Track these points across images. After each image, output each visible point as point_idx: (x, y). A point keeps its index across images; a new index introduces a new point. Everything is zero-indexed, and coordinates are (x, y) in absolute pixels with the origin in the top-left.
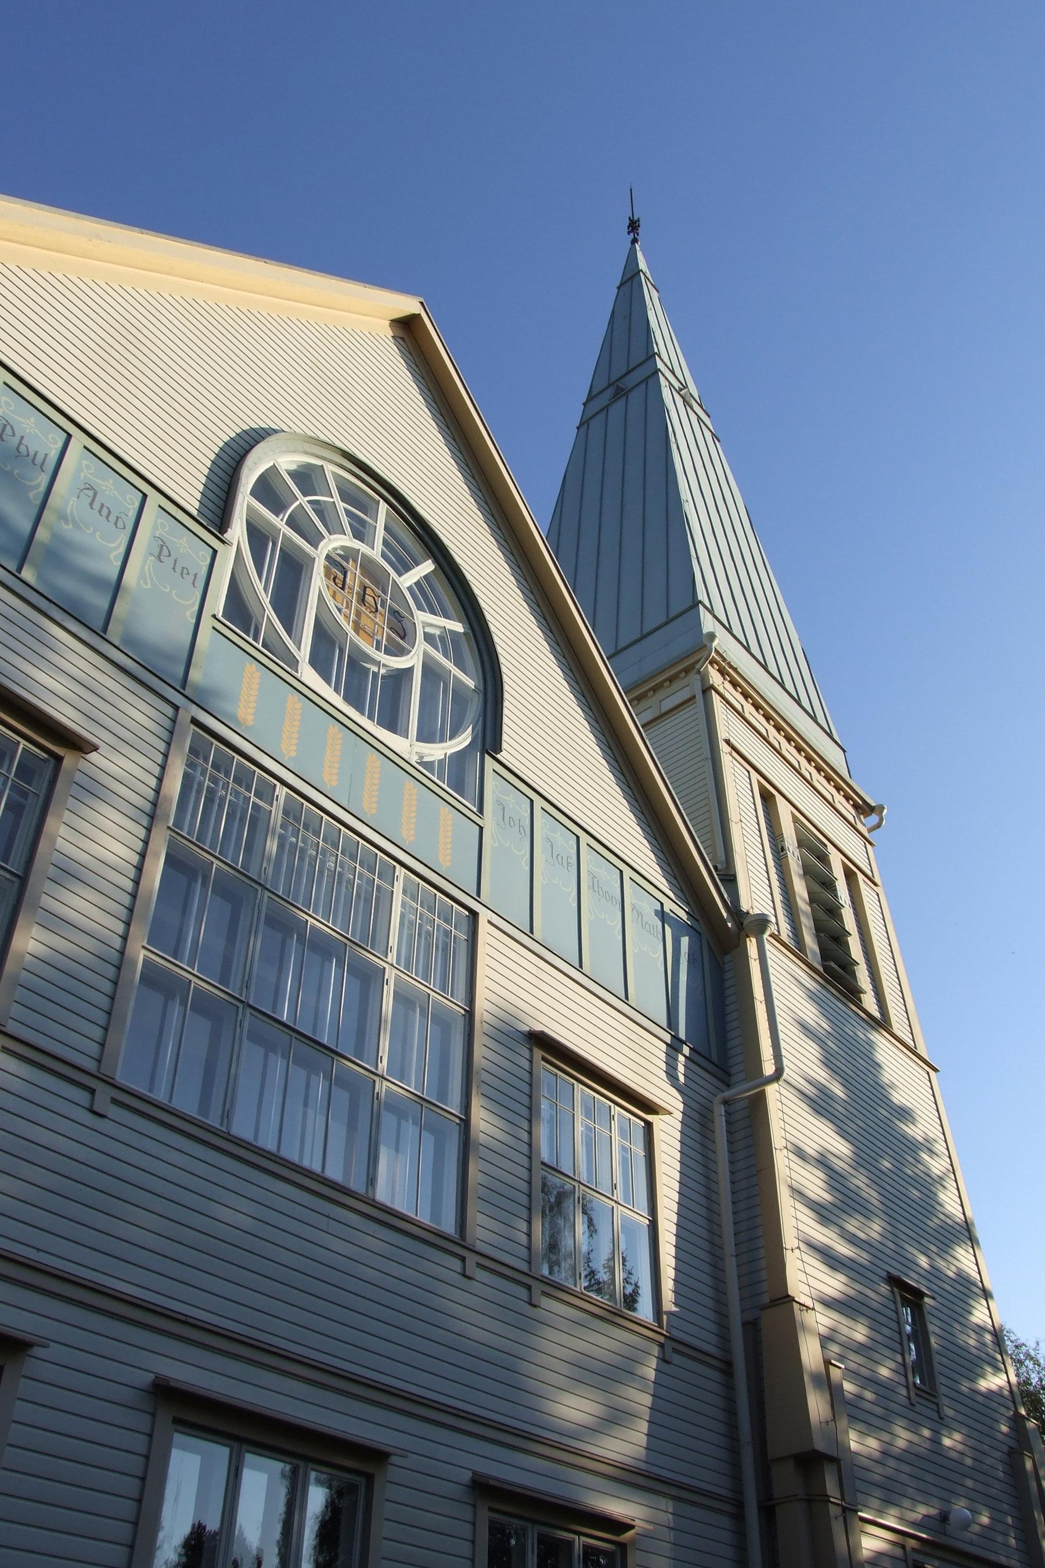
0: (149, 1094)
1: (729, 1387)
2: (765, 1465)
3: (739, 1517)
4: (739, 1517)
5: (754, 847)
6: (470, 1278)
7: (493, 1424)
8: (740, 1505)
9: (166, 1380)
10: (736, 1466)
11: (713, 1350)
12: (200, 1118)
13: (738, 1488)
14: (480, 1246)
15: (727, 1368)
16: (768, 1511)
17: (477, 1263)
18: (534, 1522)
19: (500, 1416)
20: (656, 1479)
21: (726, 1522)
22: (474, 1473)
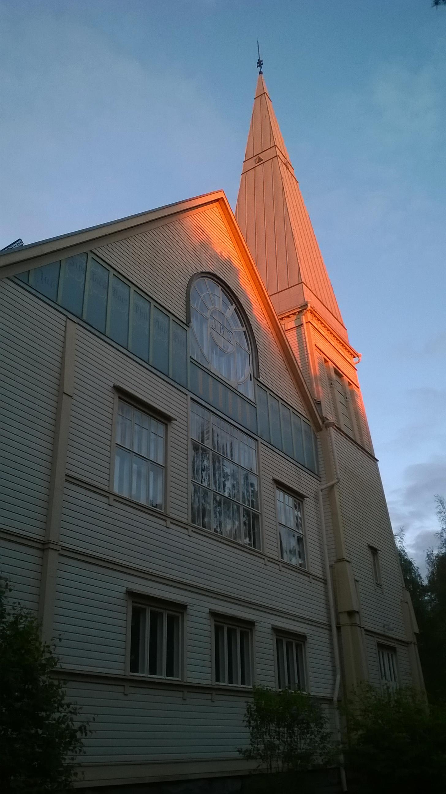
0: (259, 551)
1: (326, 588)
2: (337, 614)
3: (330, 630)
4: (330, 630)
5: (258, 335)
6: (168, 528)
7: (70, 550)
8: (330, 626)
9: (212, 610)
10: (329, 613)
11: (321, 576)
12: (234, 540)
13: (330, 621)
14: (172, 515)
15: (325, 582)
16: (339, 628)
17: (114, 499)
18: (166, 609)
19: (208, 587)
20: (306, 620)
21: (326, 632)
22: (272, 625)
